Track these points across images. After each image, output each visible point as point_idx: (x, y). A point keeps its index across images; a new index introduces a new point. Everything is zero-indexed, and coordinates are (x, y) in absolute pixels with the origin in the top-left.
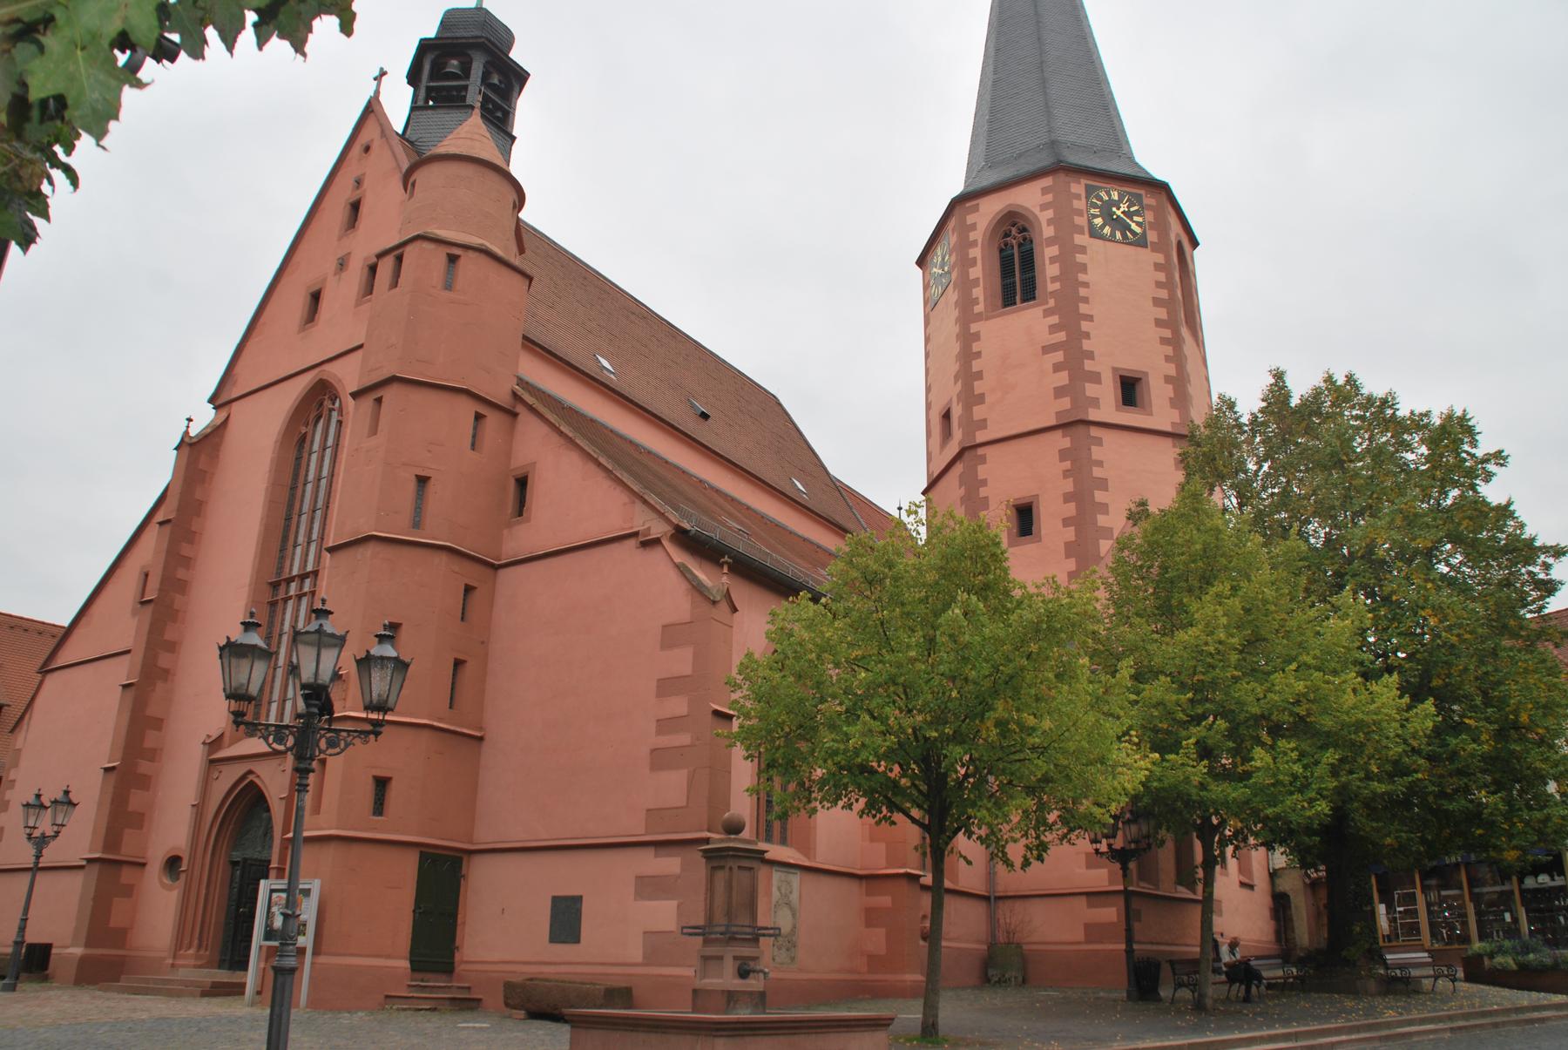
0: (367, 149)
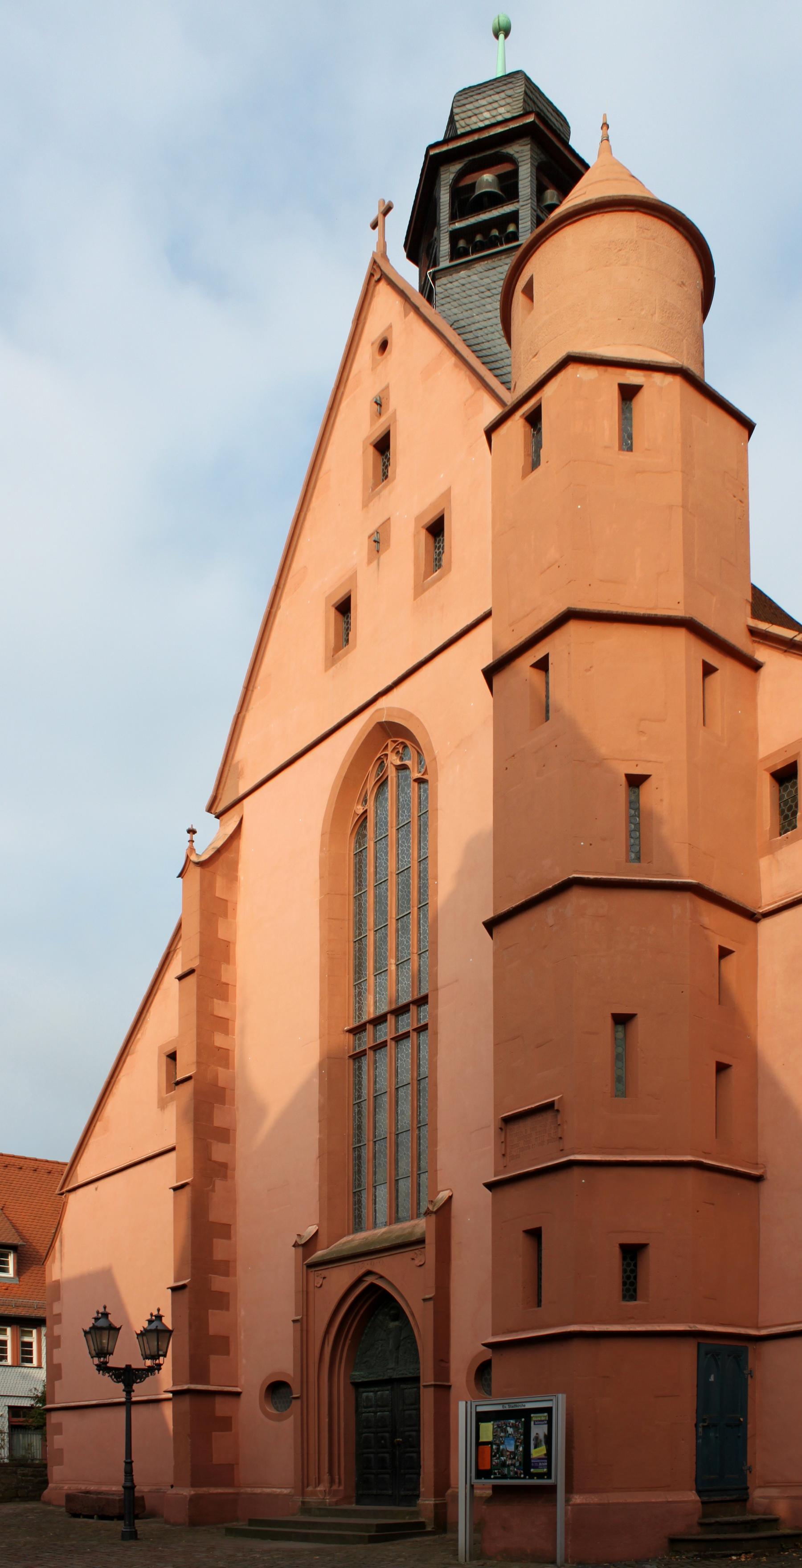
0: (384, 345)
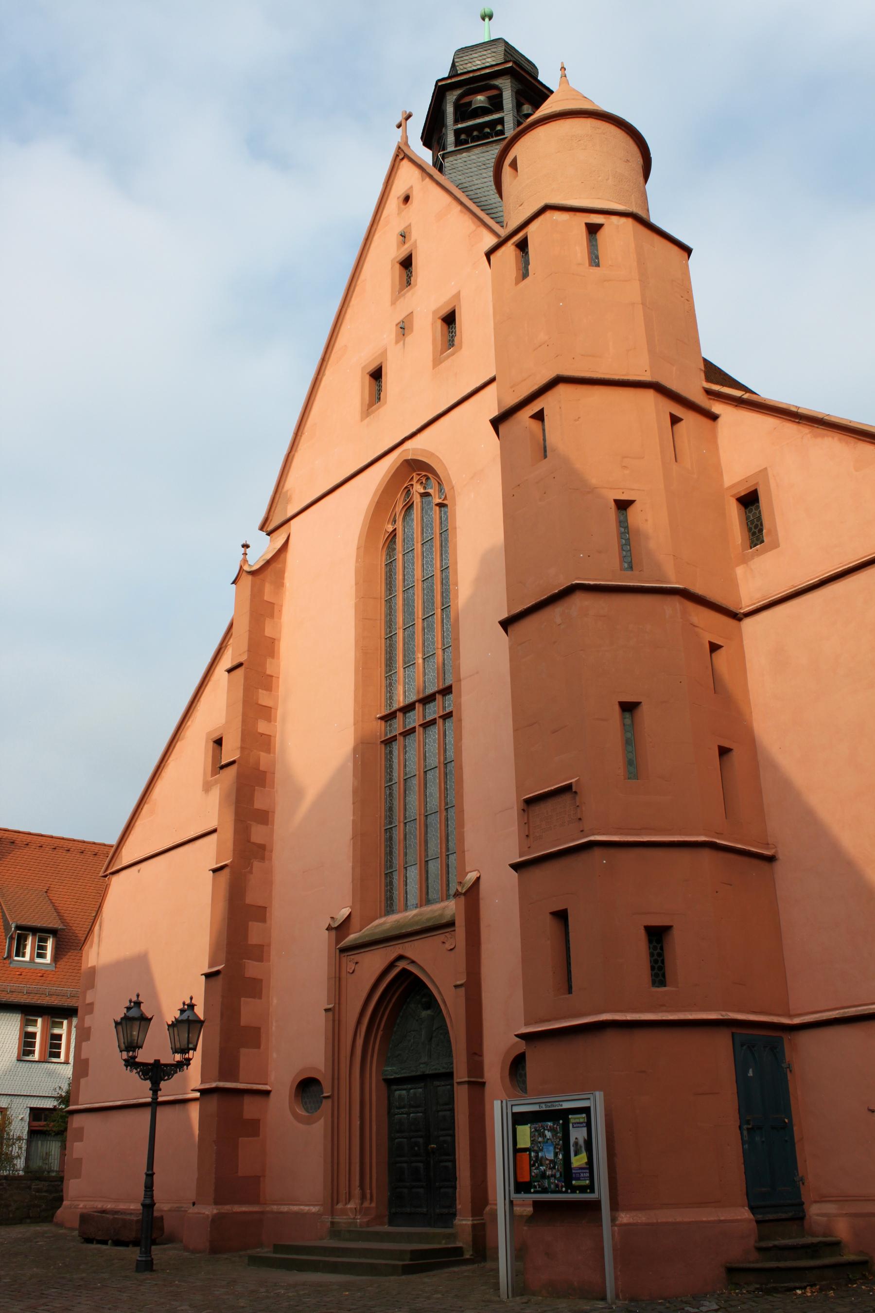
0: (407, 199)
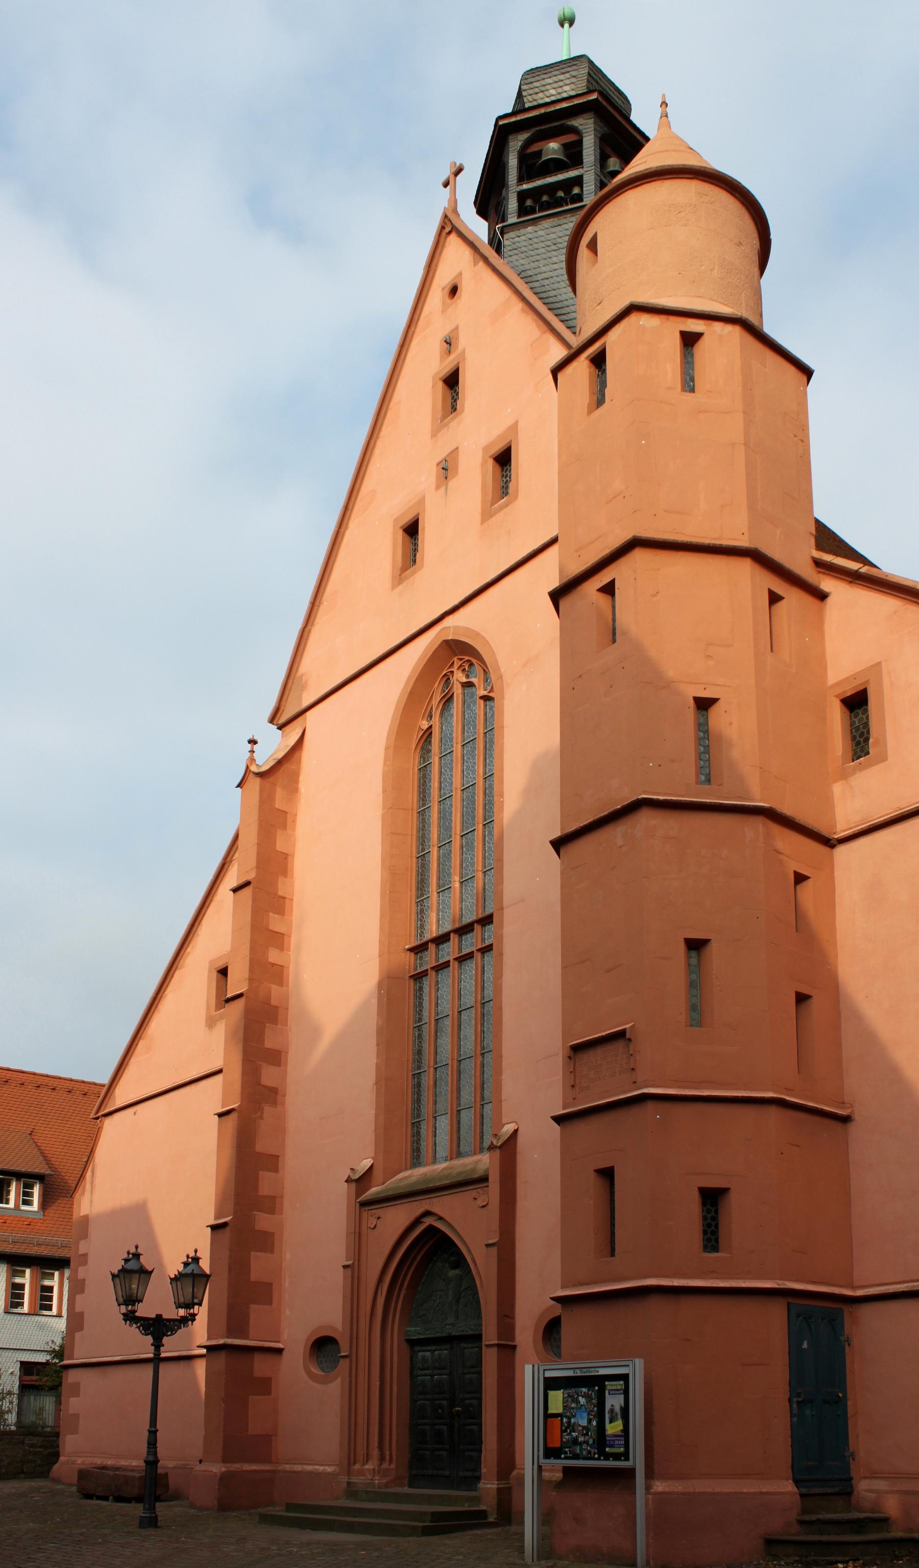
0: (454, 291)
